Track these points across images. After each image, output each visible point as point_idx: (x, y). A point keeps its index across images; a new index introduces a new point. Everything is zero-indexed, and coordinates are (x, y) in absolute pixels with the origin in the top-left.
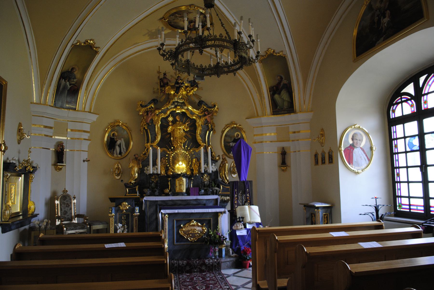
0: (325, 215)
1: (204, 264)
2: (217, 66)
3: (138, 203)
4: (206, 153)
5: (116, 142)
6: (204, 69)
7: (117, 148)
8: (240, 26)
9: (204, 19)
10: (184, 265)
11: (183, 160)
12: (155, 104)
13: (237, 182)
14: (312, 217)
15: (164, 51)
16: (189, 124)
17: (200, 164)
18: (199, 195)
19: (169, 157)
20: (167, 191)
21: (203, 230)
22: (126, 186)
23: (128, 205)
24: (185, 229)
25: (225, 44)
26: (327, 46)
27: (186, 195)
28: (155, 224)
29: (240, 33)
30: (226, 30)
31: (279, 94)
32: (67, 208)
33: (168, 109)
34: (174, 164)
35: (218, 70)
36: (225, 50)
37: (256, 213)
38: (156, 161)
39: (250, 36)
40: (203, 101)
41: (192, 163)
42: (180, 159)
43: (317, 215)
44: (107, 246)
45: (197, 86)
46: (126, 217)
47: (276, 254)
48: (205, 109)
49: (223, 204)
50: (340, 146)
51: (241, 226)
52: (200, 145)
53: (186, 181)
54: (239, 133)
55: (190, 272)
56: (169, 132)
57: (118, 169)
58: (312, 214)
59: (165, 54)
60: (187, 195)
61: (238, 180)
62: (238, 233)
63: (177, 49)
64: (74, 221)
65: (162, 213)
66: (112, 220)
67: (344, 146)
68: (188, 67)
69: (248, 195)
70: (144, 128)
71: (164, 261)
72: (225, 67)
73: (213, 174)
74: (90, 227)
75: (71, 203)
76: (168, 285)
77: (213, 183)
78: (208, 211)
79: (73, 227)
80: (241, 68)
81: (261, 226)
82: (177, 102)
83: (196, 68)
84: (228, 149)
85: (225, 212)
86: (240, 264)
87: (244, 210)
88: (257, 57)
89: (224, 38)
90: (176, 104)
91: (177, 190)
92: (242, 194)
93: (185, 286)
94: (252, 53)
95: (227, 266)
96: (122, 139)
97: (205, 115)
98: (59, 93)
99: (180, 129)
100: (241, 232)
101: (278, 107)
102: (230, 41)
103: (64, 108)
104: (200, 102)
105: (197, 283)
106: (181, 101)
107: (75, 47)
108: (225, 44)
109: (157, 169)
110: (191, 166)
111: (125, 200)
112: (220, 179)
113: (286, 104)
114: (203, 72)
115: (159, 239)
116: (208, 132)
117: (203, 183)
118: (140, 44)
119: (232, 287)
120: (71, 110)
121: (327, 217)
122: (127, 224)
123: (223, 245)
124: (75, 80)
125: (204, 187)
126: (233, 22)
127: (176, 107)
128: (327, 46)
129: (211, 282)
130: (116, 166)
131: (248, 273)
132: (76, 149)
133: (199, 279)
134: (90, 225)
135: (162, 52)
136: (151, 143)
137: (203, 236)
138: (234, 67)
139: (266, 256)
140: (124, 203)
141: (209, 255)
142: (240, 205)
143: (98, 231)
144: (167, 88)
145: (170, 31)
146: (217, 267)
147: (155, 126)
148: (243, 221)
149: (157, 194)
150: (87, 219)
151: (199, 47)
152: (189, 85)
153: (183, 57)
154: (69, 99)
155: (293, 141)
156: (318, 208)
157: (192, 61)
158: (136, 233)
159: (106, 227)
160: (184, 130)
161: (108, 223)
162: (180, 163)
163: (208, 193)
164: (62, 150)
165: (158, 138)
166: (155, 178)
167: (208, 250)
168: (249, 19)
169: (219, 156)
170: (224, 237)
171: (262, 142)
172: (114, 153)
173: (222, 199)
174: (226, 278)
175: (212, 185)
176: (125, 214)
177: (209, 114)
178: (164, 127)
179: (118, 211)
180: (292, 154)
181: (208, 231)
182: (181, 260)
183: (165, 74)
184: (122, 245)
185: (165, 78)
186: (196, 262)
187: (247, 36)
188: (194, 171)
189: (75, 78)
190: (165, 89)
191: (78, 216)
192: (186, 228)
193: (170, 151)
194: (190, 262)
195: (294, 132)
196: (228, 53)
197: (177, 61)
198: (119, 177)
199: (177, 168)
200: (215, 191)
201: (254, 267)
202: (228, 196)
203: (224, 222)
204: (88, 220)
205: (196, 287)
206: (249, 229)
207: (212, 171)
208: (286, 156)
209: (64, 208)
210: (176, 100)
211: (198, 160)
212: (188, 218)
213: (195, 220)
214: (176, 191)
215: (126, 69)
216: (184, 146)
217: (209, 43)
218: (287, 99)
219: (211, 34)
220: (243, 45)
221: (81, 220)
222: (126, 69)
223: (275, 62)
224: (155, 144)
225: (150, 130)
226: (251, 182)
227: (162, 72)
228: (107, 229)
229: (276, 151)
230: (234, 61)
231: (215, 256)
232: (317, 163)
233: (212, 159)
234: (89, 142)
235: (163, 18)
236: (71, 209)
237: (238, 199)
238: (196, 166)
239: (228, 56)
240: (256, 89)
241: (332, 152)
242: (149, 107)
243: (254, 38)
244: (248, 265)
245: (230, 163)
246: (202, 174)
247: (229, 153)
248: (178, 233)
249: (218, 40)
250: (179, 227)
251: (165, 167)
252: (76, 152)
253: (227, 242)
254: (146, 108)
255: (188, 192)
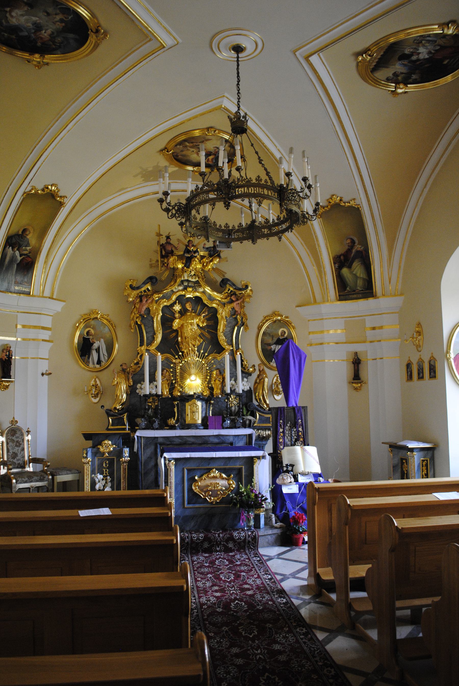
0: (423, 461)
1: (231, 538)
2: (252, 225)
3: (128, 441)
4: (233, 362)
5: (92, 344)
6: (232, 230)
7: (95, 355)
8: (288, 162)
9: (232, 150)
10: (199, 540)
11: (197, 373)
12: (153, 284)
13: (284, 408)
14: (402, 463)
15: (169, 204)
16: (206, 315)
17: (224, 379)
18: (223, 428)
19: (175, 369)
20: (172, 421)
21: (230, 484)
22: (109, 413)
23: (112, 445)
24: (203, 482)
25: (266, 192)
26: (426, 190)
27: (202, 427)
28: (153, 473)
29: (288, 175)
30: (266, 169)
31: (350, 267)
32: (17, 448)
33: (173, 292)
34: (183, 378)
35: (252, 232)
36: (265, 203)
37: (314, 458)
38: (155, 374)
39: (305, 179)
40: (228, 280)
41: (210, 377)
42: (193, 371)
43: (410, 460)
44: (83, 513)
45: (219, 256)
46: (109, 464)
47: (347, 527)
48: (232, 291)
49: (261, 443)
50: (448, 352)
51: (289, 478)
52: (224, 349)
53: (202, 406)
54: (285, 330)
55: (209, 551)
56: (175, 328)
57: (96, 388)
58: (402, 459)
59: (171, 208)
60: (204, 429)
61: (284, 404)
62: (285, 490)
63: (189, 200)
64: (27, 469)
65: (165, 458)
66: (88, 469)
67: (454, 352)
68: (206, 227)
69: (300, 429)
70: (136, 323)
71: (173, 540)
72: (264, 227)
73: (245, 395)
74: (53, 479)
75: (23, 440)
76: (181, 582)
77: (244, 408)
78: (237, 456)
79: (27, 479)
80: (290, 228)
81: (321, 478)
82: (188, 281)
83: (219, 230)
84: (268, 355)
85: (264, 457)
86: (288, 539)
87: (294, 453)
88: (315, 211)
89: (263, 182)
90: (186, 284)
91: (188, 420)
92: (291, 430)
93: (202, 573)
94: (307, 206)
95: (268, 543)
96: (102, 340)
97: (232, 302)
98: (4, 269)
99: (192, 324)
100: (290, 488)
101: (348, 289)
102: (272, 188)
103: (11, 292)
104: (223, 280)
105: (221, 570)
106: (194, 280)
107: (28, 196)
108: (266, 192)
109: (156, 387)
110: (209, 382)
111: (107, 436)
112: (255, 403)
113: (360, 283)
114: (229, 235)
115: (161, 501)
116: (236, 328)
117: (228, 409)
118: (129, 189)
119: (276, 576)
120: (22, 295)
121: (427, 465)
122: (111, 475)
123: (262, 509)
124: (28, 248)
125: (231, 415)
126: (278, 156)
127: (185, 288)
128: (426, 190)
129: (242, 568)
130: (92, 382)
131: (302, 553)
132: (30, 356)
133: (224, 562)
134: (53, 476)
135: (165, 205)
136: (147, 346)
137: (229, 495)
138: (280, 228)
139: (331, 530)
140: (106, 442)
141: (239, 525)
142: (288, 446)
143: (65, 486)
144: (171, 259)
145: (177, 169)
146: (251, 544)
147: (153, 318)
148: (292, 471)
149: (157, 427)
150: (48, 466)
151: (224, 198)
152: (206, 253)
153: (199, 214)
154: (19, 279)
155: (371, 342)
156: (412, 450)
157: (212, 219)
158: (124, 492)
159: (77, 479)
160: (198, 325)
161: (81, 472)
162: (193, 377)
163: (237, 426)
164: (9, 358)
165: (157, 338)
166: (154, 401)
167: (237, 517)
168: (304, 152)
169: (254, 366)
170: (263, 496)
171: (321, 344)
172: (89, 362)
173: (259, 435)
174: (265, 561)
175: (242, 412)
176: (108, 459)
177: (237, 300)
178: (167, 321)
179: (97, 453)
180: (370, 363)
181: (238, 486)
182: (195, 532)
183: (168, 237)
184: (106, 511)
185: (168, 243)
186: (219, 535)
187: (301, 179)
188: (215, 390)
189: (28, 245)
190: (168, 260)
191: (35, 461)
192: (202, 482)
193: (176, 358)
194: (210, 535)
195: (374, 328)
196: (269, 205)
197: (188, 219)
198: (98, 399)
199: (188, 385)
200: (248, 422)
201: (312, 544)
202: (269, 430)
203: (263, 472)
204: (49, 468)
205: (219, 575)
206: (303, 484)
207: (243, 391)
208: (360, 366)
209: (13, 449)
210: (186, 278)
211: (220, 373)
212: (205, 467)
213: (217, 469)
214: (187, 423)
215: (108, 229)
216: (198, 351)
217: (241, 191)
218: (362, 276)
219: (242, 177)
220: (294, 193)
221: (39, 467)
222: (108, 229)
223: (344, 215)
224: (153, 348)
225: (145, 326)
226: (305, 408)
227: (165, 233)
228: (78, 480)
229: (345, 358)
230: (278, 218)
231: (249, 527)
232: (410, 377)
233: (242, 371)
234: (51, 344)
235: (166, 148)
236: (23, 449)
237: (284, 436)
238: (217, 382)
239: (269, 209)
240: (313, 260)
241: (435, 360)
242: (143, 289)
243: (311, 182)
244: (301, 541)
245: (272, 377)
246: (228, 395)
247: (269, 361)
248: (190, 490)
249: (254, 185)
250: (192, 480)
251: (168, 384)
252: (30, 361)
253: (269, 504)
254: (138, 291)
255: (205, 424)
